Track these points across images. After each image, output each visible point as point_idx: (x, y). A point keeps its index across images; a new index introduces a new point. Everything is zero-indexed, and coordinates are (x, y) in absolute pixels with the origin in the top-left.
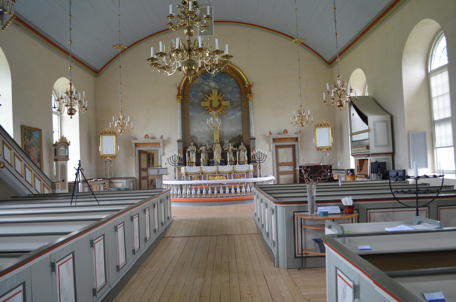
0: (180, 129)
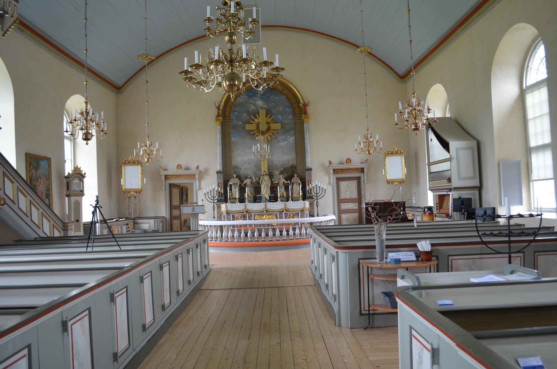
0: (220, 158)
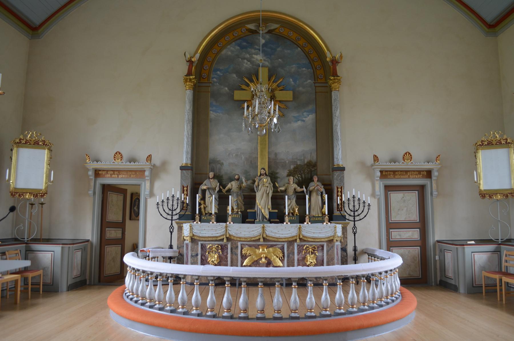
0: (187, 144)
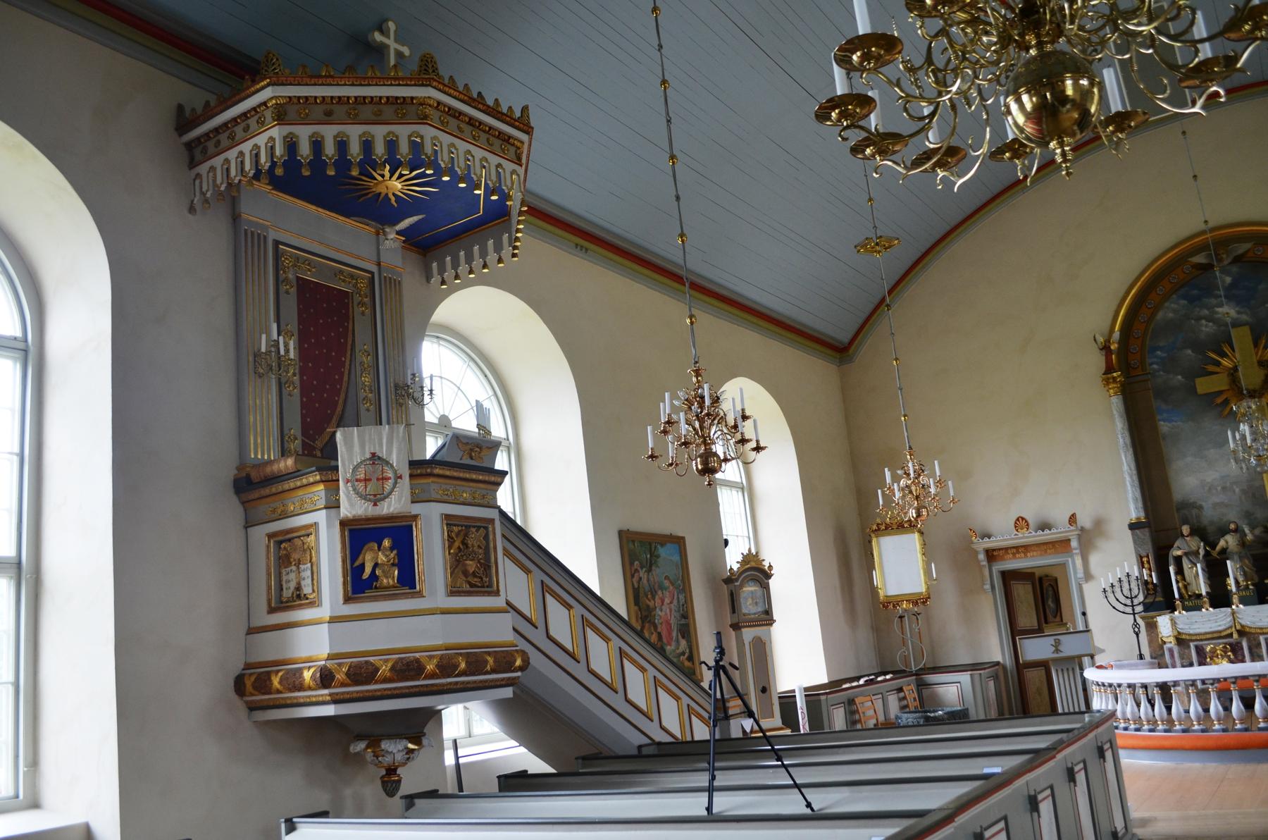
0: (1133, 486)
